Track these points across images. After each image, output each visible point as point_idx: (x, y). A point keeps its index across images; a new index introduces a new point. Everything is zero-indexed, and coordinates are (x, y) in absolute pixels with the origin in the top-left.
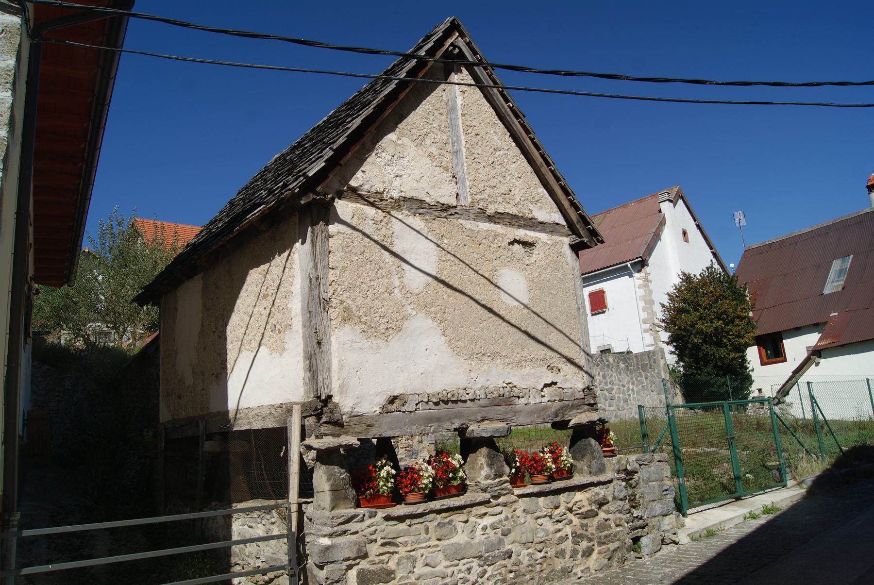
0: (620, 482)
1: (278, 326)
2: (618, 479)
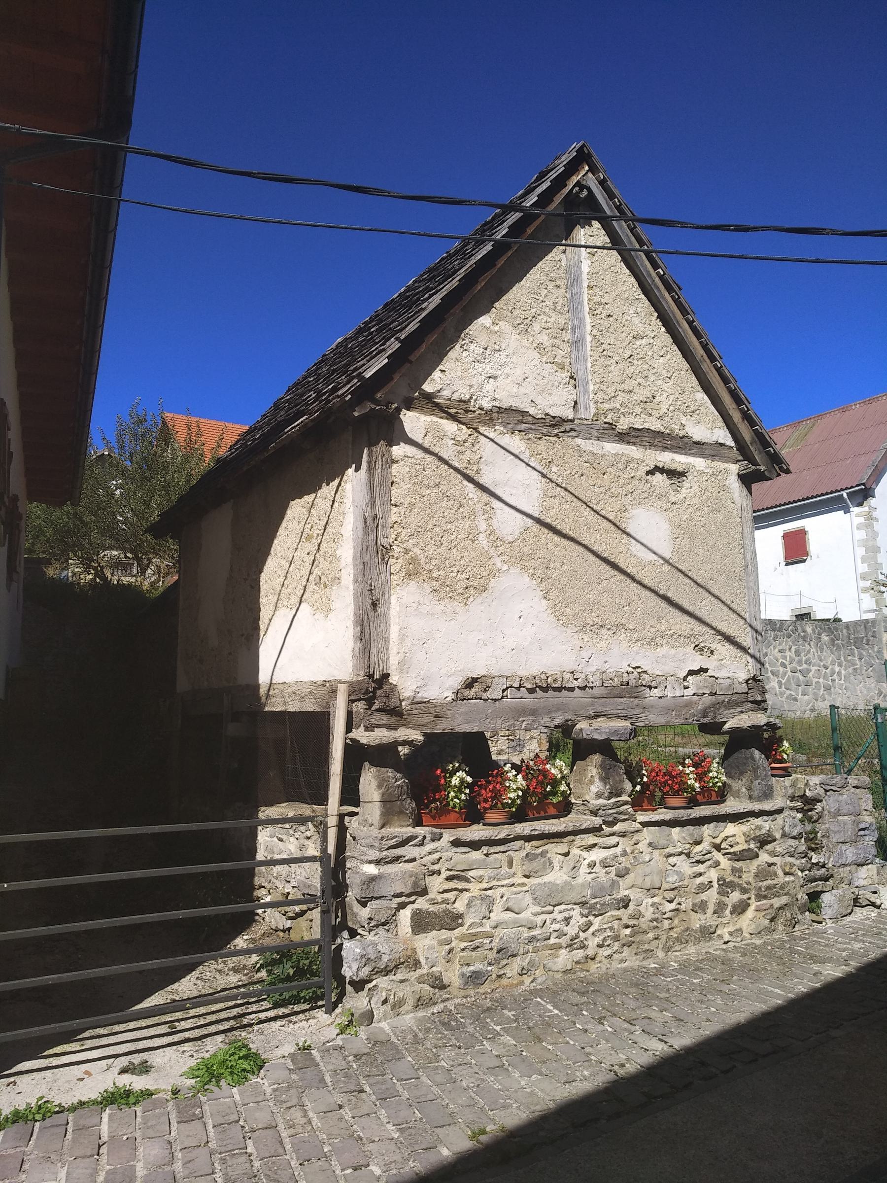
0: (794, 813)
1: (324, 579)
2: (791, 809)
